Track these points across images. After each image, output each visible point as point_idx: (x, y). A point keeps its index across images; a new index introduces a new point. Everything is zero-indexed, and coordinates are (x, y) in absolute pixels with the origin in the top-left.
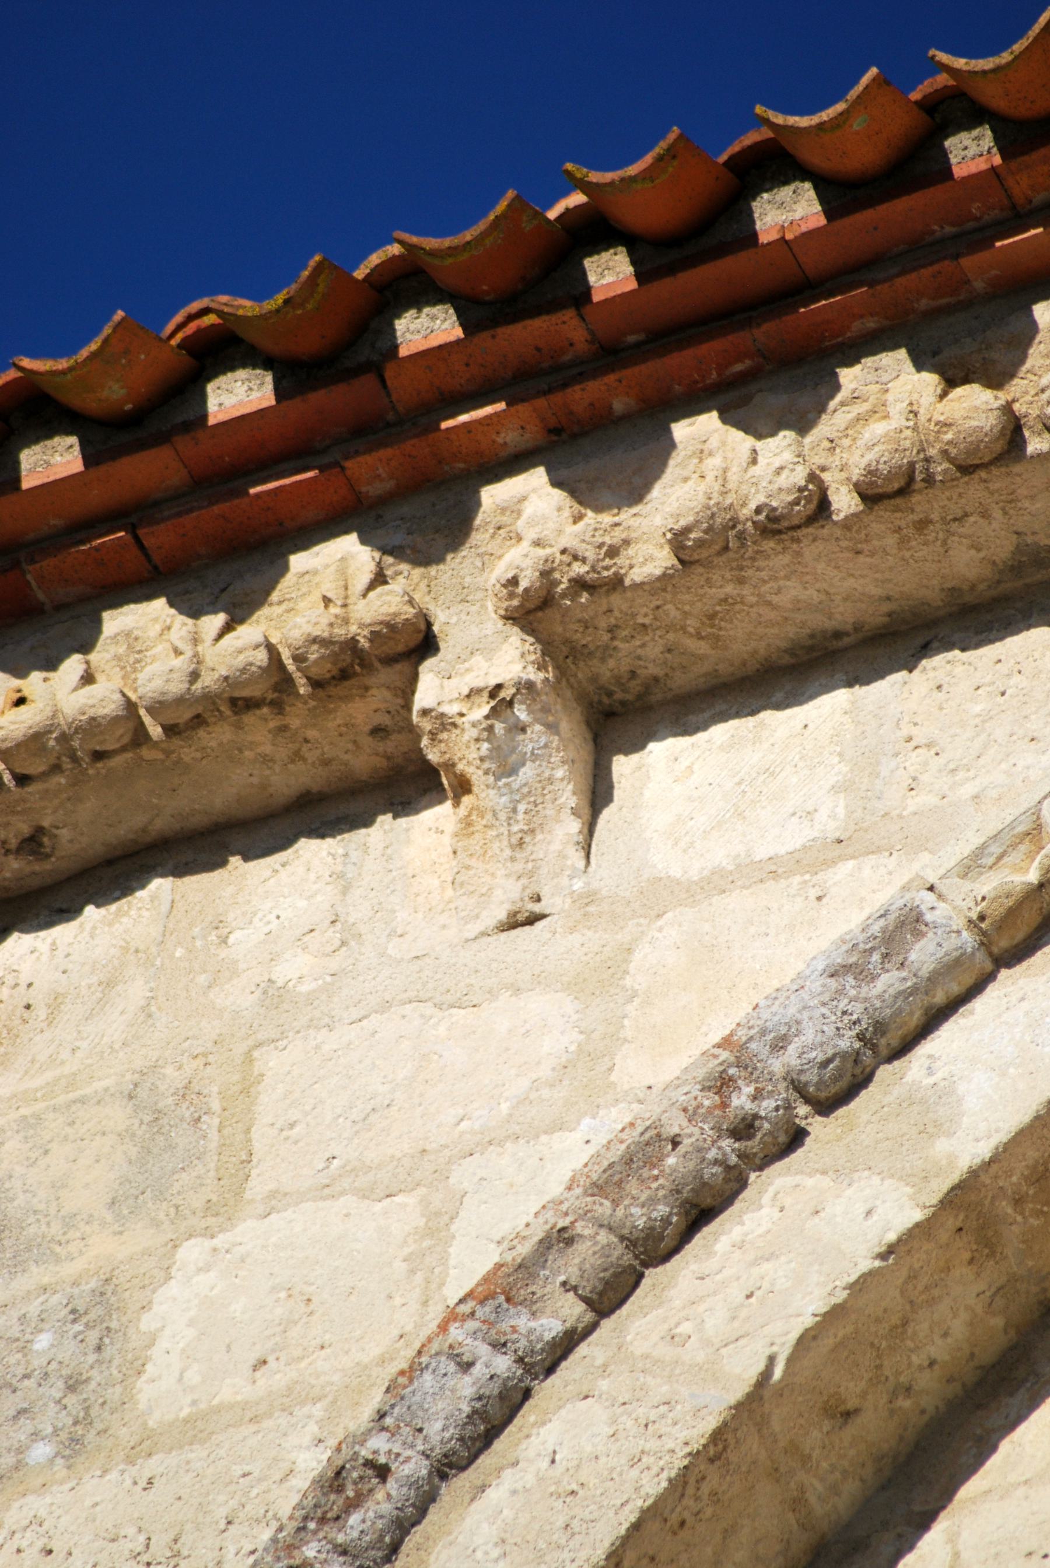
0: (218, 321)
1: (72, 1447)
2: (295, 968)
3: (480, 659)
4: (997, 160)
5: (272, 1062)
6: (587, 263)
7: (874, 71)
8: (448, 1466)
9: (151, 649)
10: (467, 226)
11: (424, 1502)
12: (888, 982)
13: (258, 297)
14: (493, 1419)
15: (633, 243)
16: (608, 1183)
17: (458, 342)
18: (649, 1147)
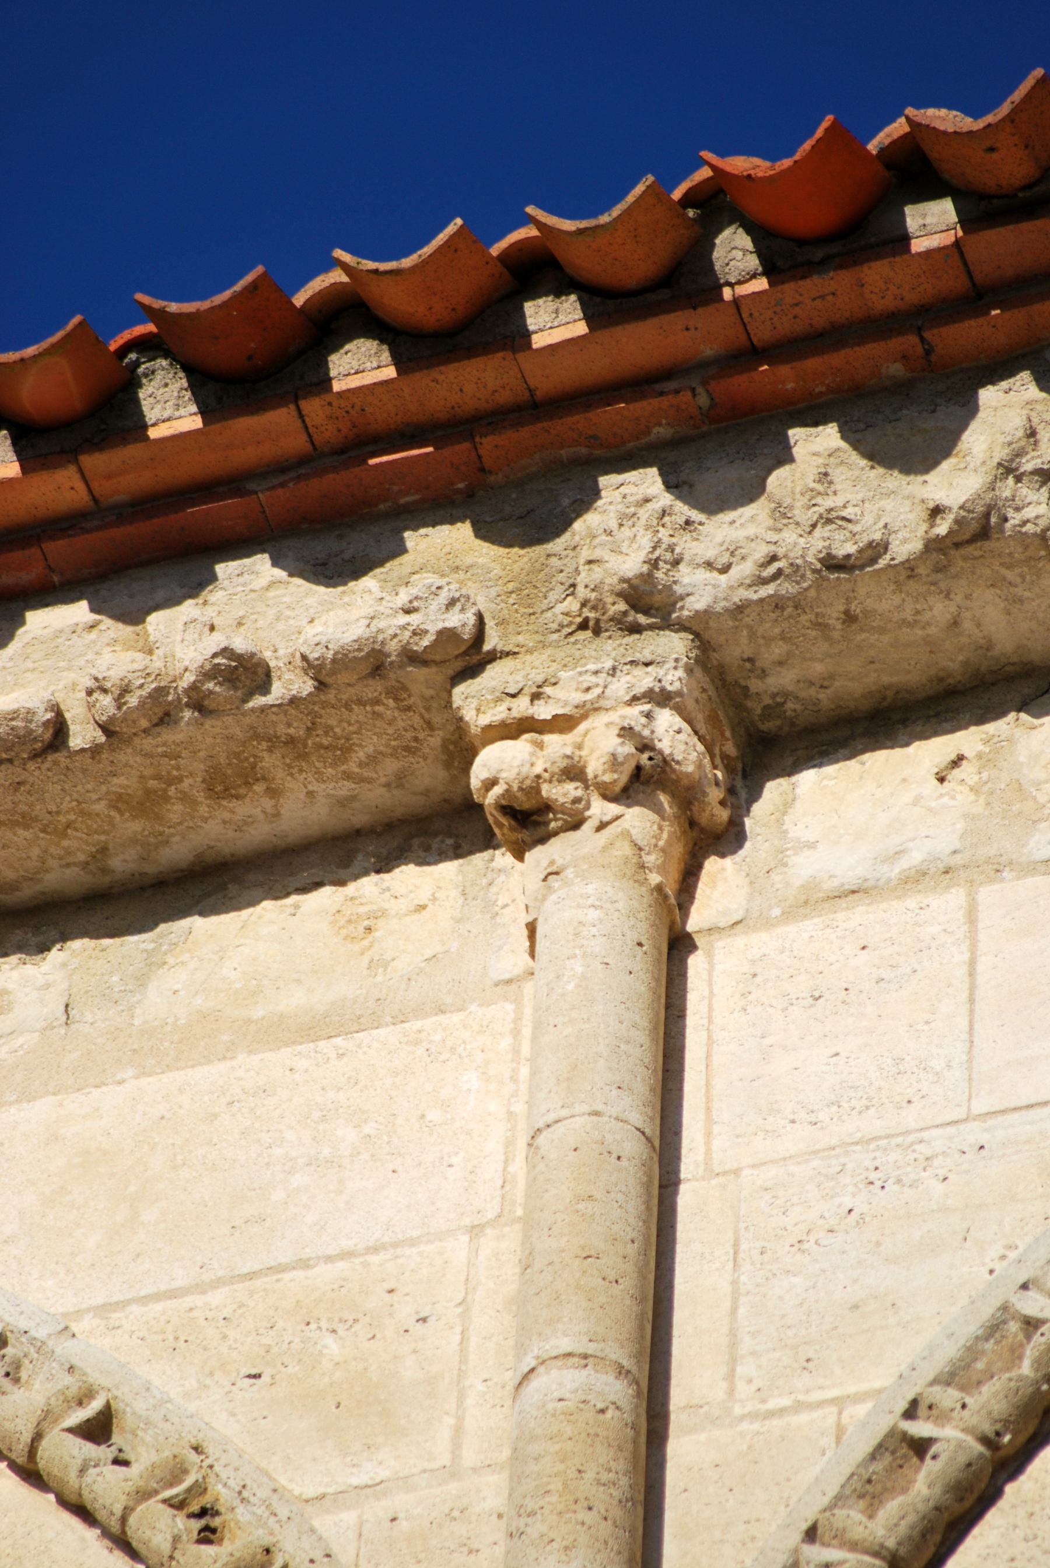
0: (345, 279)
4: (960, 233)
6: (908, 210)
7: (459, 221)
10: (407, 254)
13: (772, 156)
15: (960, 195)
17: (392, 380)
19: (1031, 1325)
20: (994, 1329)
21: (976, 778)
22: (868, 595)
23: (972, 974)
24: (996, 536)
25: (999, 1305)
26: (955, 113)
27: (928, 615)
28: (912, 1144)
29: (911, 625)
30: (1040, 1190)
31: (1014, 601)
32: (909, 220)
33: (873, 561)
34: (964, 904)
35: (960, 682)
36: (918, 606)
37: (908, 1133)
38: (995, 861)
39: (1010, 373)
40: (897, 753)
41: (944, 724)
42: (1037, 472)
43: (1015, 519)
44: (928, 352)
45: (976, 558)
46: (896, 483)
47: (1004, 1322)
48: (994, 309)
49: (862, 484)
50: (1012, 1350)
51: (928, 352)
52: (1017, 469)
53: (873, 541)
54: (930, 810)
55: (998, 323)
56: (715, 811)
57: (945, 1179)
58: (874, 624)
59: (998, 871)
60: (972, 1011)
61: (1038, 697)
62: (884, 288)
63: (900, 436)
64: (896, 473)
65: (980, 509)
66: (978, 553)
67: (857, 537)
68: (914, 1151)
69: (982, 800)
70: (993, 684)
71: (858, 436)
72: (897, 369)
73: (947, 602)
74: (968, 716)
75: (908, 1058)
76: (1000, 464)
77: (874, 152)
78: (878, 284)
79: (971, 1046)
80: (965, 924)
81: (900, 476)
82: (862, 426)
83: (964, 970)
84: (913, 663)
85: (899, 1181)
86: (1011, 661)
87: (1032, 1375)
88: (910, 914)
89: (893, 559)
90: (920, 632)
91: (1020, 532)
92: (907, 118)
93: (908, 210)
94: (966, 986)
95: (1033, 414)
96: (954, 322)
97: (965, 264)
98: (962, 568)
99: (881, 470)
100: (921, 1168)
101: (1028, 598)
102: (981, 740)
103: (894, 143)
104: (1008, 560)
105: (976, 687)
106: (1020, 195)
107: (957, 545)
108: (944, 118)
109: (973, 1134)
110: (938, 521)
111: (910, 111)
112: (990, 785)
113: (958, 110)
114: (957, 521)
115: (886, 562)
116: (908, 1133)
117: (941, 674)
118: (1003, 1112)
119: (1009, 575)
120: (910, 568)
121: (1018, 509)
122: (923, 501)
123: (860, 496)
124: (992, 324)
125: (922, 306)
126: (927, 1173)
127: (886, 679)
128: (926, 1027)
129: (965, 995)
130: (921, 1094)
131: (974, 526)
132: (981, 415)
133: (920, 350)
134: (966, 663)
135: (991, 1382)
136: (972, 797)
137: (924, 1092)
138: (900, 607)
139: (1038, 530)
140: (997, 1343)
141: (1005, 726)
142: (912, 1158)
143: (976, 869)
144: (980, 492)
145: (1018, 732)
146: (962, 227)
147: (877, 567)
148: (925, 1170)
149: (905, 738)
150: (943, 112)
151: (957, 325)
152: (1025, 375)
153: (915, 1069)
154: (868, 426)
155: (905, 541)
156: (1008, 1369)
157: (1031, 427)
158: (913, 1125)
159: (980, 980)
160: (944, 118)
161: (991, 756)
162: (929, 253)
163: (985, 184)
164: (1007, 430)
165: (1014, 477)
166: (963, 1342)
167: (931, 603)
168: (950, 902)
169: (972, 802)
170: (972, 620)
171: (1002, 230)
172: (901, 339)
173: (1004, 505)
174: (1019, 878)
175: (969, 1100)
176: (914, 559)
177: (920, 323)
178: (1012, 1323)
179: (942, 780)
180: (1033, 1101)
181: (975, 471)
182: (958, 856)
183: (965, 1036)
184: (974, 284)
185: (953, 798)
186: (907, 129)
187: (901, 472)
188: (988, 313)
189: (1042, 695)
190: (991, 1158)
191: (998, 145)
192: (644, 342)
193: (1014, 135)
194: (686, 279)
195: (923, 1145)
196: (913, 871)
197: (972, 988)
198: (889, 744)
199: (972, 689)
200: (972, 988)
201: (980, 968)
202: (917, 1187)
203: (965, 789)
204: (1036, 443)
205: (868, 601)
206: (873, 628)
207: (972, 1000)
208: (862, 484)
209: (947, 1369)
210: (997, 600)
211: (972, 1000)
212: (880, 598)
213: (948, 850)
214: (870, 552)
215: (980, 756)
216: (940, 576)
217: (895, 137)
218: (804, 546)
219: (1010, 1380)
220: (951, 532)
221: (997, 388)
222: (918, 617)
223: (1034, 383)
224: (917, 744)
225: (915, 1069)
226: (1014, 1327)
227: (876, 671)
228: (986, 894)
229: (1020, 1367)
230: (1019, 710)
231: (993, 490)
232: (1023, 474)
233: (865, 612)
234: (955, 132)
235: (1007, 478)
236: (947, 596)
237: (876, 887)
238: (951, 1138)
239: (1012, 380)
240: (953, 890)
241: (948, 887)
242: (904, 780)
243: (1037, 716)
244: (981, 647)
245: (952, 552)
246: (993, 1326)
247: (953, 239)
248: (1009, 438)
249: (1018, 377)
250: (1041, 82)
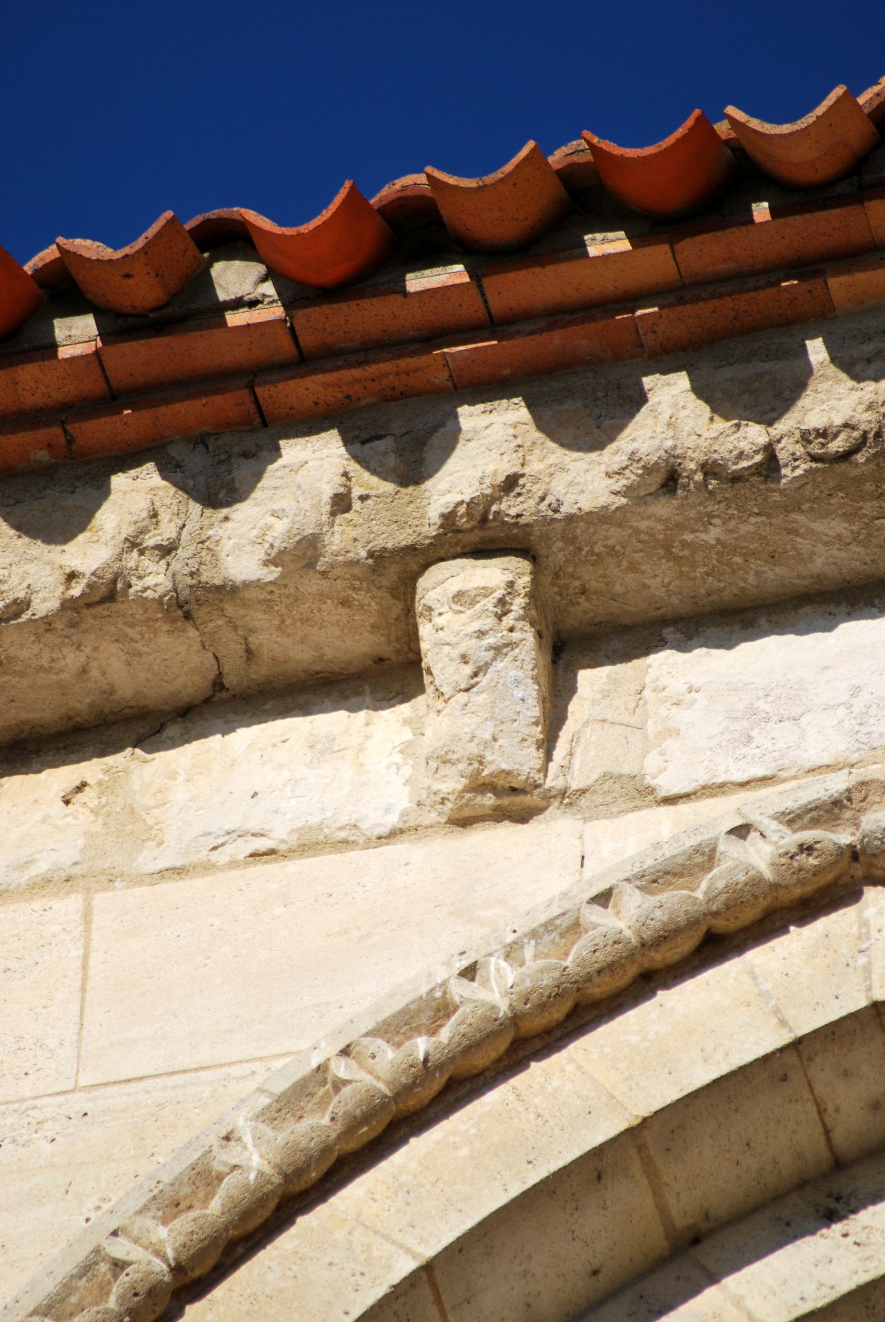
4: (100, 344)
6: (57, 322)
7: (531, 144)
19: (119, 1266)
20: (86, 1269)
21: (96, 802)
22: (12, 644)
23: (85, 967)
24: (121, 599)
25: (92, 1249)
26: (98, 243)
27: (61, 663)
28: (27, 1109)
29: (47, 671)
30: (133, 1152)
31: (134, 654)
32: (57, 331)
33: (17, 615)
34: (82, 908)
35: (86, 720)
36: (54, 655)
37: (24, 1100)
38: (109, 873)
39: (139, 464)
40: (31, 777)
41: (72, 756)
42: (157, 547)
43: (137, 585)
44: (70, 442)
45: (103, 617)
46: (39, 551)
47: (96, 1263)
48: (126, 409)
49: (10, 550)
50: (101, 1288)
51: (70, 442)
52: (140, 544)
53: (18, 598)
54: (56, 827)
55: (129, 422)
57: (53, 1140)
58: (16, 669)
59: (111, 881)
60: (83, 999)
61: (151, 736)
62: (34, 387)
63: (44, 511)
64: (39, 542)
65: (109, 576)
66: (105, 613)
67: (4, 594)
68: (28, 1116)
69: (100, 821)
70: (114, 724)
71: (9, 509)
72: (43, 455)
73: (78, 653)
74: (91, 750)
75: (27, 1037)
76: (126, 539)
77: (29, 273)
78: (191, 350)
79: (81, 1029)
80: (81, 924)
81: (42, 545)
82: (12, 501)
83: (79, 963)
84: (47, 703)
85: (14, 1141)
86: (130, 704)
87: (116, 1309)
88: (35, 915)
89: (34, 615)
90: (54, 677)
91: (141, 596)
92: (58, 246)
93: (57, 322)
94: (79, 977)
95: (156, 499)
96: (92, 418)
97: (103, 370)
98: (92, 625)
99: (26, 539)
100: (33, 1130)
101: (146, 653)
102: (102, 770)
103: (46, 266)
104: (130, 620)
105: (99, 725)
106: (151, 315)
107: (88, 605)
108: (89, 248)
109: (79, 1102)
110: (73, 584)
111: (60, 240)
112: (107, 808)
113: (100, 241)
114: (89, 586)
115: (27, 617)
116: (24, 1100)
117: (70, 713)
118: (105, 1085)
119: (131, 632)
120: (47, 623)
121: (140, 578)
122: (61, 567)
123: (8, 561)
124: (125, 421)
125: (66, 403)
126: (38, 1135)
127: (24, 716)
128: (44, 1011)
129: (78, 985)
130: (36, 1068)
131: (103, 591)
132: (112, 497)
133: (63, 440)
134: (91, 705)
135: (81, 1314)
136: (92, 818)
137: (39, 1066)
138: (38, 656)
139: (157, 596)
140: (88, 1281)
141: (122, 759)
142: (26, 1122)
143: (93, 879)
144: (109, 562)
145: (133, 765)
146: (101, 339)
147: (20, 620)
148: (36, 1132)
149: (38, 766)
150: (88, 242)
151: (94, 421)
152: (150, 466)
153: (33, 1047)
154: (17, 502)
155: (44, 600)
156: (97, 1304)
157: (154, 510)
158: (28, 1094)
159: (92, 972)
160: (89, 248)
161: (109, 784)
162: (73, 360)
163: (122, 304)
164: (134, 511)
165: (139, 550)
166: (60, 1279)
167: (64, 653)
168: (68, 906)
169: (92, 822)
170: (99, 669)
171: (135, 344)
172: (47, 430)
173: (129, 574)
174: (128, 888)
175: (77, 1074)
176: (52, 615)
177: (63, 418)
178: (102, 1264)
179: (67, 802)
180: (130, 1076)
181: (106, 544)
182: (78, 867)
183: (77, 1020)
184: (110, 388)
185: (76, 818)
186: (57, 255)
187: (43, 542)
188: (122, 412)
189: (155, 734)
190: (93, 1124)
191: (134, 273)
192: (139, 358)
193: (147, 265)
194: (194, 306)
195: (36, 1111)
196: (39, 878)
197: (85, 979)
198: (24, 770)
199: (96, 726)
200: (85, 979)
201: (92, 962)
202: (29, 1147)
203: (86, 811)
204: (157, 523)
205: (12, 648)
206: (15, 671)
207: (83, 989)
208: (10, 550)
209: (45, 1302)
210: (120, 653)
211: (83, 989)
212: (22, 646)
213: (69, 862)
214: (14, 608)
215: (100, 783)
216: (73, 630)
217: (47, 261)
219: (98, 1312)
220: (83, 595)
221: (126, 475)
222: (54, 665)
223: (157, 472)
224: (48, 771)
225: (33, 1047)
226: (103, 1267)
227: (16, 708)
228: (100, 900)
229: (107, 1302)
230: (135, 746)
231: (120, 560)
232: (145, 548)
233: (8, 658)
234: (98, 260)
235: (132, 551)
236: (79, 648)
237: (7, 891)
238: (59, 1106)
239: (139, 470)
240: (72, 896)
241: (69, 893)
242: (36, 801)
243: (149, 752)
244: (105, 692)
245: (84, 611)
246: (86, 1266)
247: (94, 349)
248: (135, 518)
249: (144, 467)
250: (533, 151)
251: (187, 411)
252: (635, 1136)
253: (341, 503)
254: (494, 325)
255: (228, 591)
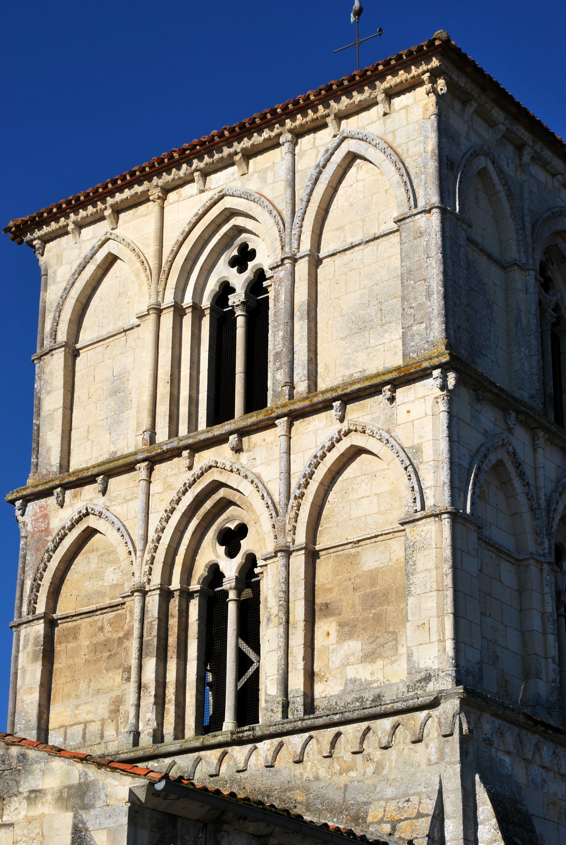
1: (54, 283)
2: (65, 246)
3: (71, 227)
5: (64, 253)
8: (71, 287)
9: (54, 226)
11: (70, 290)
12: (93, 251)
14: (73, 284)
16: (79, 267)
18: (81, 264)
55: (153, 174)
56: (164, 198)
78: (164, 165)
168: (177, 204)
218: (165, 181)
251: (176, 164)
252: (212, 222)
253: (187, 170)
254: (193, 154)
255: (181, 177)
